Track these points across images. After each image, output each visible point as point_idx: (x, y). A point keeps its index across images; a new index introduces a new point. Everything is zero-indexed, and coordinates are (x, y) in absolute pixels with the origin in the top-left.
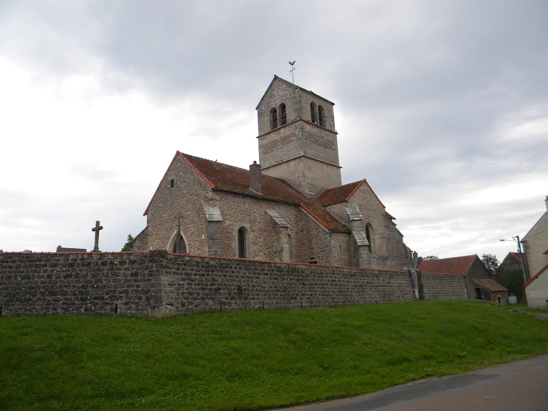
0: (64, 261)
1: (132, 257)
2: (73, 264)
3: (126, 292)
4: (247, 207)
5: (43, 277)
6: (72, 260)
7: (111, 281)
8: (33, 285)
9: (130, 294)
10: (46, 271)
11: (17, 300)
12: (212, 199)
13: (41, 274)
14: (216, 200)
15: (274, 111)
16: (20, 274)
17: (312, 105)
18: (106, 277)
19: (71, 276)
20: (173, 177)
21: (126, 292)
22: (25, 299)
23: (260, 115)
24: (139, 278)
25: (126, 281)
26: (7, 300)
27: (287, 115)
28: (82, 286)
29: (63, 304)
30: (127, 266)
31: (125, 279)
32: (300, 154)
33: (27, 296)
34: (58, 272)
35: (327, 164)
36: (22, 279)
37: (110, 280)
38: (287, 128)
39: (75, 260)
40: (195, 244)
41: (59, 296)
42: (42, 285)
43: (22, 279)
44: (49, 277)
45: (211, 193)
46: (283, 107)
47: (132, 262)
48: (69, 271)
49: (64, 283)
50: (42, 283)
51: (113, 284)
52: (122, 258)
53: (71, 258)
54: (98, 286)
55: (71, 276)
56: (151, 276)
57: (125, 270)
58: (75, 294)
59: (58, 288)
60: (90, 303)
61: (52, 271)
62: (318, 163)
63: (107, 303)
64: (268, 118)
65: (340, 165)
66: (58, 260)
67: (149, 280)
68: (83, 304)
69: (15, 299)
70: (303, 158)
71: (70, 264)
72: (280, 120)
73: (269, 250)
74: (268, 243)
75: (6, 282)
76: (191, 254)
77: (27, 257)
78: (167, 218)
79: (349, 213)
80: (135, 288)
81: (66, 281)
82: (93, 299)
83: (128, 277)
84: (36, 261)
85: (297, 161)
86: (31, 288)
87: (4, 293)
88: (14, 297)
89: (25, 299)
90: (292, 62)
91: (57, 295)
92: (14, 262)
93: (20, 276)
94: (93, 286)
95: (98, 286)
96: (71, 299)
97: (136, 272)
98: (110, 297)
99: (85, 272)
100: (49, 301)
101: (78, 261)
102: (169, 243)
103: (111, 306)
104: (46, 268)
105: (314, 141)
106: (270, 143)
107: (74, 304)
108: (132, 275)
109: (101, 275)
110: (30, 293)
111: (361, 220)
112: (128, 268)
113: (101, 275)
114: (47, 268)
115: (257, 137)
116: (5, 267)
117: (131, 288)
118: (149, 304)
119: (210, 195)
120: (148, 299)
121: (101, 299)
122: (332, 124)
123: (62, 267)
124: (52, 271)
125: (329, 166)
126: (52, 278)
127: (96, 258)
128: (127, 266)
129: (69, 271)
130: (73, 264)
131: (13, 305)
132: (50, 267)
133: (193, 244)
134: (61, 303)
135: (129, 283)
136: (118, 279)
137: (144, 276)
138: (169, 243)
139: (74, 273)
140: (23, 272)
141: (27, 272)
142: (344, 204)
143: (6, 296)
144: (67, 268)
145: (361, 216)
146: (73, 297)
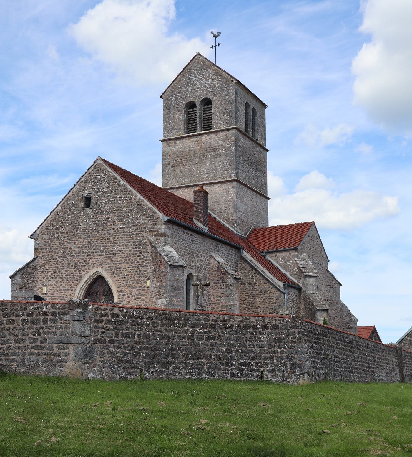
0: (205, 320)
1: (274, 322)
2: (215, 325)
3: (271, 358)
4: (195, 248)
5: (184, 338)
6: (213, 320)
7: (256, 346)
8: (174, 347)
9: (275, 361)
10: (186, 331)
11: (159, 363)
12: (163, 235)
13: (182, 334)
14: (168, 236)
15: (191, 105)
16: (159, 333)
17: (247, 105)
18: (250, 341)
19: (214, 338)
20: (90, 192)
21: (271, 358)
22: (167, 362)
23: (167, 108)
24: (283, 343)
25: (271, 347)
26: (148, 362)
27: (213, 116)
28: (227, 350)
29: (209, 369)
30: (270, 330)
31: (269, 345)
32: (230, 177)
33: (169, 358)
34: (200, 333)
35: (257, 192)
36: (162, 338)
37: (254, 345)
38: (213, 136)
39: (216, 321)
40: (131, 291)
41: (203, 360)
42: (184, 347)
43: (162, 338)
44: (190, 338)
45: (163, 226)
46: (207, 102)
47: (275, 327)
48: (211, 333)
49: (207, 345)
50: (183, 345)
51: (258, 349)
52: (265, 322)
53: (211, 318)
54: (242, 351)
55: (214, 338)
56: (294, 342)
57: (268, 334)
58: (220, 359)
59: (201, 352)
60: (236, 369)
61: (193, 332)
62: (249, 191)
63: (253, 370)
64: (180, 116)
65: (269, 196)
66: (199, 320)
67: (292, 347)
68: (228, 370)
69: (155, 361)
70: (235, 183)
71: (211, 325)
72: (200, 121)
73: (213, 306)
74: (212, 297)
75: (145, 341)
76: (124, 303)
77: (164, 314)
78: (77, 250)
79: (300, 266)
80: (279, 355)
81: (209, 343)
82: (239, 364)
83: (272, 343)
84: (175, 320)
85: (226, 186)
86: (172, 349)
87: (143, 353)
88: (154, 358)
89: (167, 362)
90: (215, 33)
91: (200, 358)
92: (151, 318)
93: (159, 335)
94: (237, 351)
95: (242, 351)
96: (216, 364)
97: (279, 338)
98: (256, 363)
99: (228, 335)
100: (193, 365)
101: (220, 322)
102: (81, 285)
103: (257, 373)
104: (186, 328)
105: (246, 159)
106: (182, 152)
107: (219, 369)
108: (276, 340)
109: (245, 339)
110: (172, 355)
111: (316, 277)
112: (271, 333)
113: (245, 339)
114: (187, 328)
115: (162, 141)
116: (140, 324)
117: (275, 355)
118: (295, 372)
119: (162, 228)
120: (293, 366)
121: (246, 366)
122: (264, 136)
123: (204, 328)
124: (193, 332)
125: (259, 196)
126: (194, 340)
127: (238, 320)
128: (270, 330)
129: (211, 333)
130: (215, 325)
131: (154, 368)
132: (190, 327)
133: (126, 290)
134: (205, 367)
135: (273, 350)
136: (263, 344)
137: (287, 342)
138: (81, 285)
139: (217, 336)
140: (161, 331)
141: (166, 330)
142: (293, 253)
143: (146, 358)
144: (208, 329)
145: (315, 271)
146: (218, 361)
